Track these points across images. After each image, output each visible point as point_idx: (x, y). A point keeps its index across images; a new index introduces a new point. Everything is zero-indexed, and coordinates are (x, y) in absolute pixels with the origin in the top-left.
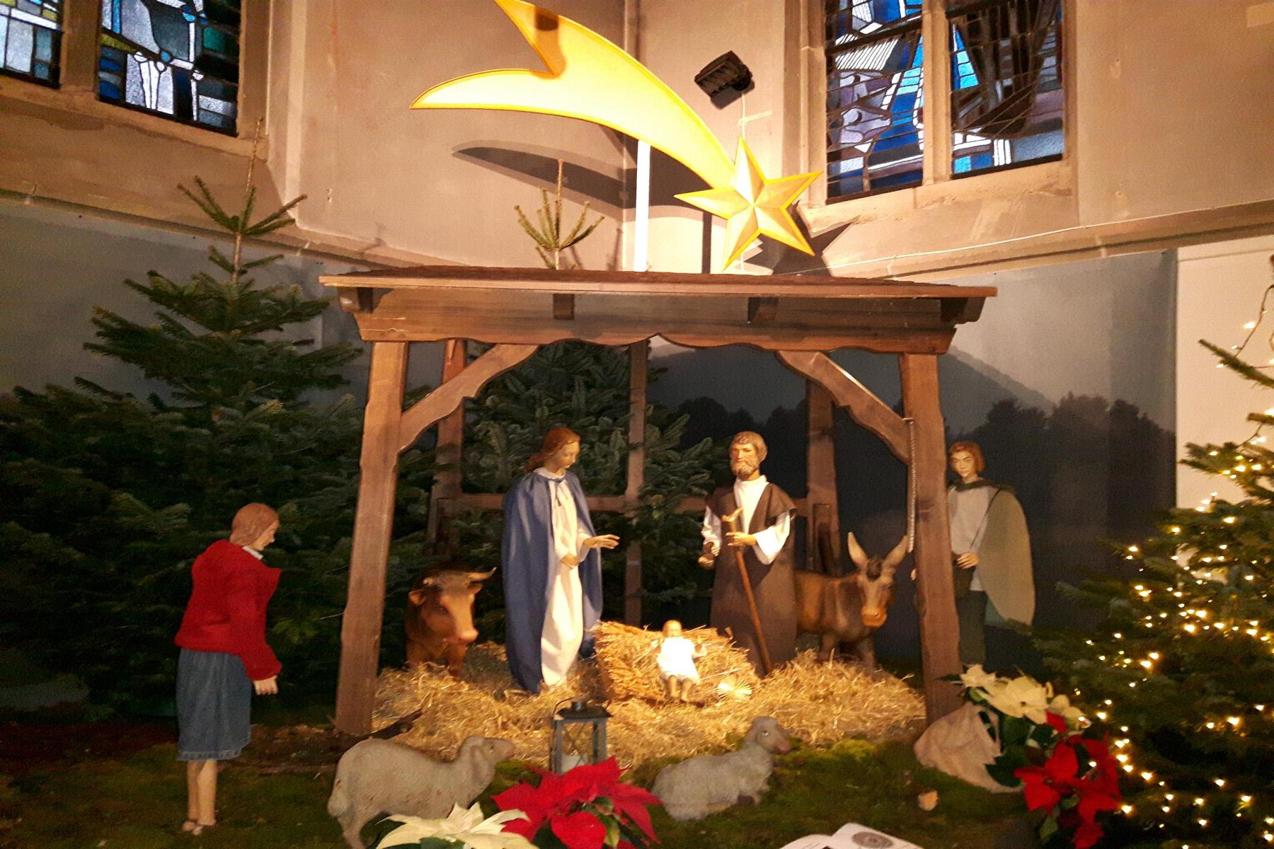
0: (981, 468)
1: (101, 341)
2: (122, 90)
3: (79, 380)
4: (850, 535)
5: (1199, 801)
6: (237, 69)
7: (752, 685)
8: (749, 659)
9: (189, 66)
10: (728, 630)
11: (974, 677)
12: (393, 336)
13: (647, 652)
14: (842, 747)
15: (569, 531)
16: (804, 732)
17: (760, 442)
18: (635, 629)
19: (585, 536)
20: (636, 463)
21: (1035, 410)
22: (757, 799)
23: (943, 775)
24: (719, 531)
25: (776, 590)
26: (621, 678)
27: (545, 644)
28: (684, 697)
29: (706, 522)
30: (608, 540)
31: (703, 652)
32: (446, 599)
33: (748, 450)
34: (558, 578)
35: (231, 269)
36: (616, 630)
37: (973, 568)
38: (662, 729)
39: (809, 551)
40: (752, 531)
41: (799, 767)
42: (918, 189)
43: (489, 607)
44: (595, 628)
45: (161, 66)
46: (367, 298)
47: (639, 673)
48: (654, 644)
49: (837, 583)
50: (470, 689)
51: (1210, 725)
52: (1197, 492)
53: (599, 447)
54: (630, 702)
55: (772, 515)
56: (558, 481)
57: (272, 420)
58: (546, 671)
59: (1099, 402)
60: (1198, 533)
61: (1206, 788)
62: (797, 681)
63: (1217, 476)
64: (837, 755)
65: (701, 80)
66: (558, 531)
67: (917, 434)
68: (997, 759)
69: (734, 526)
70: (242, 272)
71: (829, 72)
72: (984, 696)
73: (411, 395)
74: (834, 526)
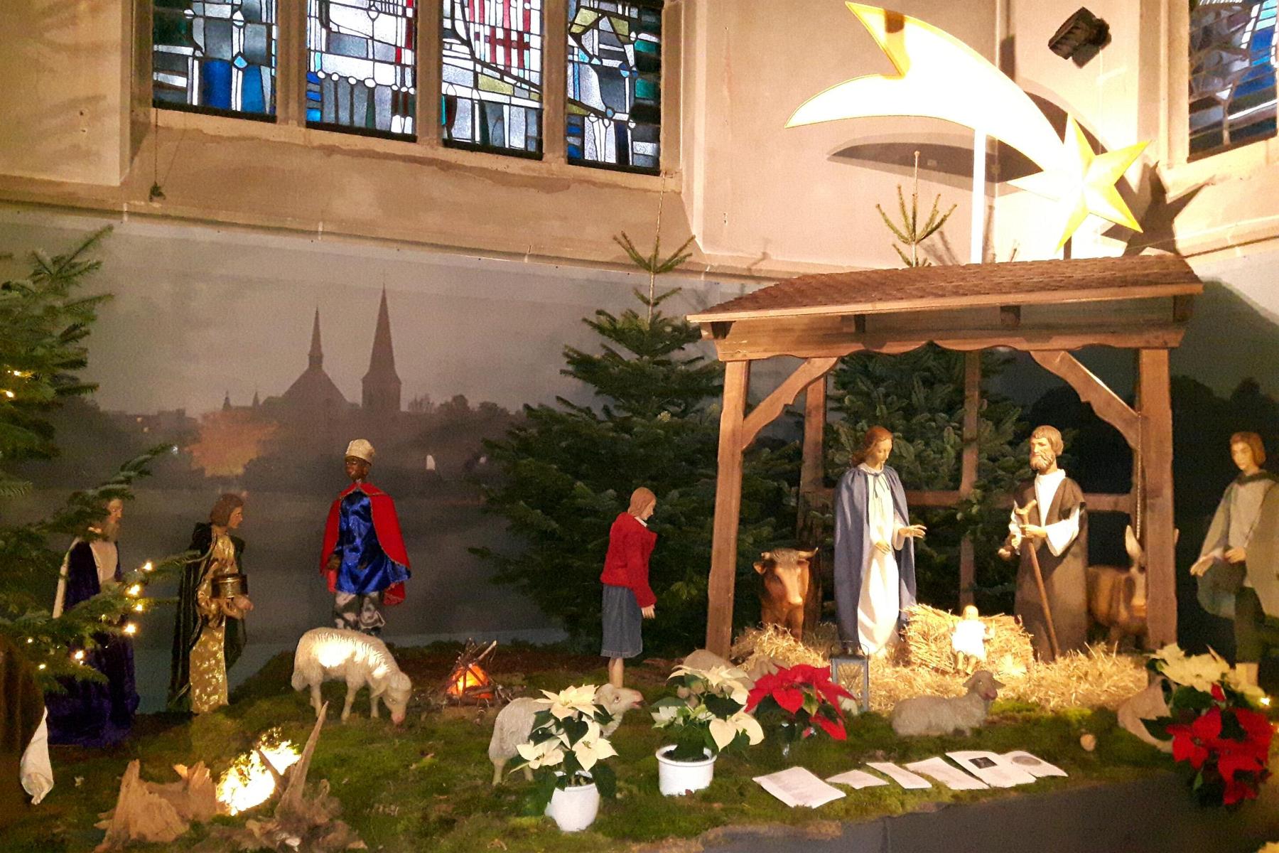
1: (570, 368)
2: (582, 149)
3: (559, 398)
6: (659, 110)
9: (625, 117)
12: (739, 356)
13: (943, 630)
18: (942, 612)
19: (899, 525)
22: (968, 734)
26: (919, 650)
27: (861, 615)
30: (918, 530)
31: (992, 634)
32: (780, 571)
34: (874, 561)
35: (648, 303)
40: (1049, 522)
42: (1272, 140)
45: (606, 121)
46: (721, 330)
47: (933, 647)
53: (935, 444)
56: (876, 475)
57: (665, 426)
60: (791, 486)
65: (1055, 45)
70: (656, 304)
71: (1191, 9)
73: (748, 408)
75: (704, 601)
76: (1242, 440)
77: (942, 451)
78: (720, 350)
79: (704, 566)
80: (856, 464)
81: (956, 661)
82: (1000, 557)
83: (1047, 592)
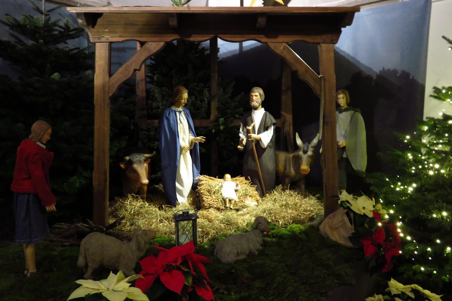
0: (349, 101)
4: (297, 134)
5: (429, 249)
7: (257, 201)
8: (257, 190)
10: (249, 177)
11: (344, 196)
12: (103, 40)
13: (217, 188)
14: (291, 228)
15: (186, 135)
16: (276, 221)
17: (261, 92)
18: (213, 178)
19: (192, 137)
20: (214, 104)
21: (369, 76)
23: (331, 240)
24: (246, 134)
25: (268, 159)
26: (208, 199)
27: (177, 185)
28: (232, 207)
29: (241, 130)
30: (200, 138)
31: (239, 188)
33: (257, 96)
34: (182, 156)
35: (41, 13)
36: (205, 179)
37: (344, 148)
38: (221, 222)
39: (281, 142)
41: (274, 237)
43: (153, 170)
44: (197, 178)
48: (220, 184)
49: (291, 155)
50: (149, 205)
51: (434, 216)
52: (434, 109)
54: (210, 210)
55: (266, 126)
56: (180, 112)
58: (178, 196)
59: (395, 71)
61: (432, 244)
62: (275, 199)
63: (444, 102)
64: (290, 231)
66: (181, 135)
67: (324, 83)
68: (353, 234)
69: (251, 131)
72: (348, 205)
74: (291, 132)
75: (90, 186)
76: (343, 93)
77: (202, 101)
78: (92, 34)
79: (88, 165)
80: (169, 107)
81: (225, 203)
82: (237, 149)
83: (260, 164)
